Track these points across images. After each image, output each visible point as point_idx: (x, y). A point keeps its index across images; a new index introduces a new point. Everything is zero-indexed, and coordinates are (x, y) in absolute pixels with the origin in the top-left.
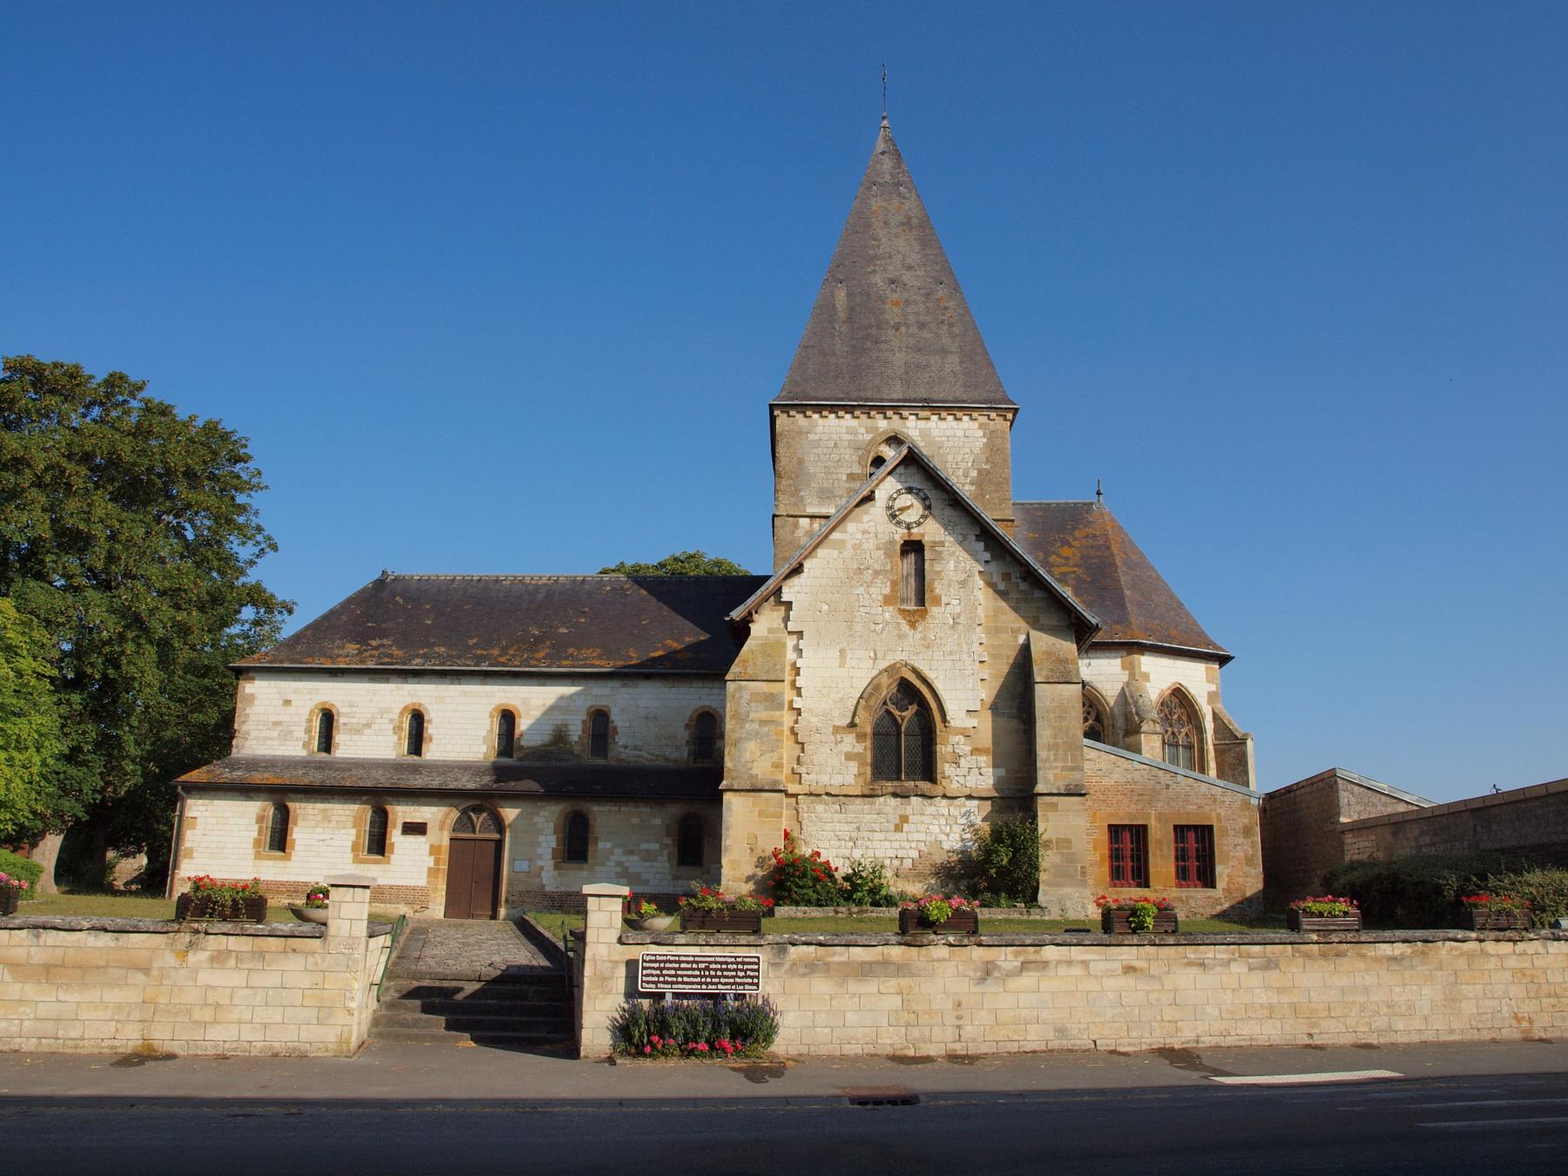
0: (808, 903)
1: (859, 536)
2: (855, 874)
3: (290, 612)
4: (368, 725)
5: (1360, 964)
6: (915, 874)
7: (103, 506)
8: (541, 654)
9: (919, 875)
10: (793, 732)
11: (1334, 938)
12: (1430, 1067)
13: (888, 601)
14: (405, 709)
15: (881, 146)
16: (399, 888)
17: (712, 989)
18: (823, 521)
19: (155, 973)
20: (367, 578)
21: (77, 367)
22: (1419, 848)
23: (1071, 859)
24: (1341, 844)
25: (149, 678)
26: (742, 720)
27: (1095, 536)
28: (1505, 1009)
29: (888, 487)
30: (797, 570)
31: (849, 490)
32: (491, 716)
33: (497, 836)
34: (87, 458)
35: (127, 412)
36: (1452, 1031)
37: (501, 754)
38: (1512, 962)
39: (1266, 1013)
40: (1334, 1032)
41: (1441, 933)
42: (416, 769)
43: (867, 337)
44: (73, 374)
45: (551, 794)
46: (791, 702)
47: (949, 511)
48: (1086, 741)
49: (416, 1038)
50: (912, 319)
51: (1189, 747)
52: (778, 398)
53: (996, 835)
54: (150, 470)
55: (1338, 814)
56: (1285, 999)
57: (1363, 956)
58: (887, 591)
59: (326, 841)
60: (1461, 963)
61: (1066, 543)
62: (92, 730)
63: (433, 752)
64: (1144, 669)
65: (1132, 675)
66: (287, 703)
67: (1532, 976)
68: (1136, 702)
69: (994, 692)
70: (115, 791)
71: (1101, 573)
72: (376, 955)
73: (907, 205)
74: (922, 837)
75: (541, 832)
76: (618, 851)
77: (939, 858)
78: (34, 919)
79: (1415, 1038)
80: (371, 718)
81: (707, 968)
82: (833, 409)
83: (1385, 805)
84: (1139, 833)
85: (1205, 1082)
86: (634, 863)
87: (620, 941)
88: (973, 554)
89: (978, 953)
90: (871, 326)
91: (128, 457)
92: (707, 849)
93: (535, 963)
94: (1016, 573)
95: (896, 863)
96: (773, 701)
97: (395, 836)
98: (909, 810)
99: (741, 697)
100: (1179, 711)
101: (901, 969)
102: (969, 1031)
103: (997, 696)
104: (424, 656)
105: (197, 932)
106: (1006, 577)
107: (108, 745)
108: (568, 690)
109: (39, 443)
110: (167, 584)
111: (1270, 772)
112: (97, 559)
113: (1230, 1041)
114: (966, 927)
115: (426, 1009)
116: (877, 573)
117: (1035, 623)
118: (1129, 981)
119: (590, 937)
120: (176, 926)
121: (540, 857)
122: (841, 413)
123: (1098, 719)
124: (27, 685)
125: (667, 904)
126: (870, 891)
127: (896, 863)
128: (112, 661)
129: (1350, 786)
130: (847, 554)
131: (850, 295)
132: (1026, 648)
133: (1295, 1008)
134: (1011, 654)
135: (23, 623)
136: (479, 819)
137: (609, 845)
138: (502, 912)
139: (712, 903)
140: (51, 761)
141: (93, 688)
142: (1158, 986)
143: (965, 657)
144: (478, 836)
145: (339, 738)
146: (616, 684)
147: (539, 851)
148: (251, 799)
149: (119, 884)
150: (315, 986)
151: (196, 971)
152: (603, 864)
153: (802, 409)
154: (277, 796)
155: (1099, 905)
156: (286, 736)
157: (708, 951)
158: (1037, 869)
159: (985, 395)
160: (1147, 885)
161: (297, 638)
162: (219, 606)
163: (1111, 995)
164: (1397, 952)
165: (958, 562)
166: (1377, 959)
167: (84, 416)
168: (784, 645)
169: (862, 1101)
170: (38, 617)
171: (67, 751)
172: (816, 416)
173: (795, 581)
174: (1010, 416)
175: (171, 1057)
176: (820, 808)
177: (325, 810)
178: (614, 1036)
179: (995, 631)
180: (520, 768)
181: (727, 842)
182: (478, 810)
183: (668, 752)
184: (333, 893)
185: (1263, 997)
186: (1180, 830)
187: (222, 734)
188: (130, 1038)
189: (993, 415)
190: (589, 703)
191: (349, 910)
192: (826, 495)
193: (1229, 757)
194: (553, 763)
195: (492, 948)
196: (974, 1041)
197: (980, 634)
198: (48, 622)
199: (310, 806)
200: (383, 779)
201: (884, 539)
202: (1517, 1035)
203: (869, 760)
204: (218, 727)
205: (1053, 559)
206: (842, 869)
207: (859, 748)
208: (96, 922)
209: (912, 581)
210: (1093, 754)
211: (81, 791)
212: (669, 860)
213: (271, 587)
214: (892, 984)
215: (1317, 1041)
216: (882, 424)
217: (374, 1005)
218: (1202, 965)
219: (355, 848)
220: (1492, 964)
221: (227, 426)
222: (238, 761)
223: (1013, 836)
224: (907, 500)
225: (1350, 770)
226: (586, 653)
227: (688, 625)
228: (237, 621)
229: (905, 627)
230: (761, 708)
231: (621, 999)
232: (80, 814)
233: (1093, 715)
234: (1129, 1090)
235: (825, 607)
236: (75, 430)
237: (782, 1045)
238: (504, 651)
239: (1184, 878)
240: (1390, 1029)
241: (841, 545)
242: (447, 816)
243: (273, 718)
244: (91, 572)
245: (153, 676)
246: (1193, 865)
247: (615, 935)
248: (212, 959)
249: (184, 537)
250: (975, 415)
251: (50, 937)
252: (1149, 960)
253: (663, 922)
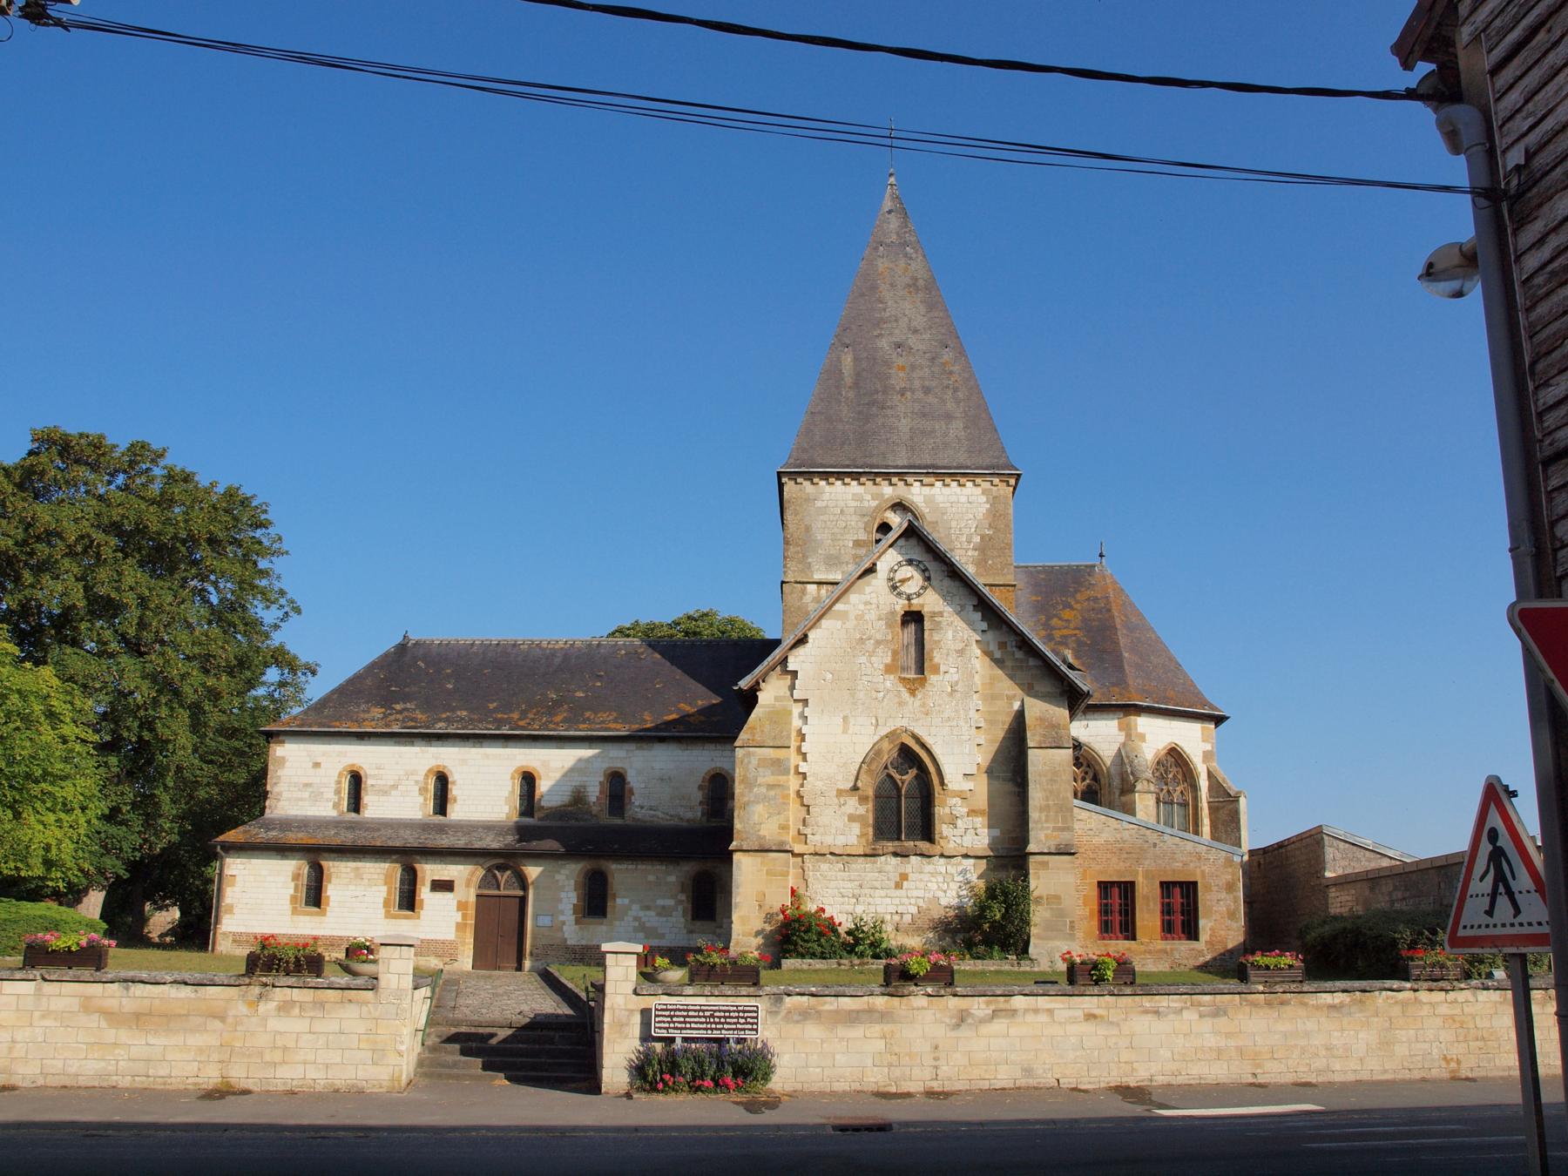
0: (813, 955)
1: (862, 607)
2: (857, 929)
3: (314, 673)
4: (395, 787)
5: (1302, 1012)
6: (913, 928)
7: (133, 575)
8: (559, 718)
9: (918, 929)
10: (799, 795)
11: (1278, 988)
12: (1353, 1102)
13: (889, 669)
14: (430, 771)
15: (888, 204)
16: (429, 942)
17: (716, 1034)
18: (830, 587)
19: (230, 1020)
20: (388, 643)
21: (101, 437)
22: (1392, 902)
23: (1061, 914)
24: (1326, 898)
25: (182, 741)
26: (750, 785)
27: (1096, 599)
28: (1435, 1051)
29: (890, 559)
30: (803, 640)
31: (855, 557)
32: (513, 778)
33: (521, 893)
34: (115, 528)
35: (151, 480)
36: (1385, 1071)
37: (522, 814)
38: (1444, 1010)
39: (1214, 1055)
40: (1276, 1072)
41: (1378, 984)
42: (441, 829)
43: (874, 403)
44: (97, 444)
45: (571, 853)
46: (797, 767)
47: (947, 582)
48: (1077, 802)
49: (457, 1077)
50: (917, 383)
51: (1184, 805)
52: (787, 465)
53: (991, 893)
54: (175, 537)
55: (1324, 869)
56: (1232, 1043)
57: (1306, 1004)
58: (888, 660)
59: (358, 901)
60: (1396, 1011)
61: (1068, 606)
62: (129, 792)
63: (458, 812)
64: (1140, 730)
65: (1128, 736)
66: (317, 765)
67: (1462, 1023)
68: (1131, 763)
69: (990, 757)
70: (150, 848)
71: (1101, 639)
72: (419, 1006)
73: (913, 265)
74: (921, 893)
76: (636, 907)
77: (937, 913)
78: (124, 974)
79: (1351, 1077)
80: (398, 779)
81: (712, 1016)
82: (840, 476)
83: (1369, 860)
84: (1127, 889)
85: (1147, 1114)
86: (651, 918)
87: (635, 993)
88: (970, 624)
89: (953, 1002)
90: (877, 392)
91: (154, 526)
92: (719, 905)
93: (560, 1012)
94: (1011, 641)
95: (896, 918)
96: (779, 766)
98: (908, 869)
99: (749, 761)
100: (1174, 770)
101: (885, 1016)
102: (945, 1070)
103: (993, 761)
104: (447, 720)
105: (266, 985)
106: (1002, 645)
107: (146, 806)
108: (586, 753)
109: (68, 514)
110: (196, 650)
111: (1257, 832)
112: (129, 622)
113: (1181, 1080)
114: (943, 978)
115: (464, 1052)
116: (878, 643)
117: (1030, 690)
118: (1089, 1028)
119: (609, 989)
120: (247, 980)
121: (562, 912)
122: (847, 480)
123: (1095, 778)
124: (72, 750)
125: (677, 956)
126: (872, 944)
127: (896, 918)
128: (147, 724)
129: (1335, 842)
130: (851, 624)
131: (856, 359)
132: (1020, 717)
133: (1240, 1050)
134: (1006, 720)
135: (66, 691)
136: (504, 877)
137: (626, 901)
138: (527, 964)
139: (716, 958)
140: (94, 821)
141: (131, 751)
142: (1115, 1031)
143: (962, 723)
144: (503, 892)
145: (367, 799)
146: (631, 746)
147: (560, 907)
149: (155, 936)
150: (369, 1032)
151: (265, 1019)
153: (809, 476)
154: (312, 856)
155: (1064, 960)
156: (316, 797)
157: (713, 1001)
158: (1028, 924)
159: (987, 461)
160: (1134, 938)
161: (324, 703)
162: (244, 668)
163: (1073, 1040)
164: (1337, 1001)
165: (955, 631)
166: (1318, 1007)
167: (109, 483)
168: (790, 713)
169: (843, 1129)
170: (75, 683)
171: (107, 811)
172: (823, 483)
173: (801, 650)
174: (1012, 482)
175: (246, 1092)
176: (824, 867)
178: (631, 1075)
179: (991, 698)
180: (544, 829)
181: (736, 899)
182: (502, 868)
183: (681, 812)
184: (384, 953)
185: (1212, 1041)
186: (1166, 886)
187: (253, 793)
188: (211, 1077)
189: (996, 480)
190: (605, 765)
191: (396, 966)
192: (832, 561)
193: (1223, 815)
194: (573, 823)
195: (517, 999)
196: (950, 1079)
197: (977, 702)
198: (85, 686)
200: (410, 839)
201: (885, 610)
202: (1446, 1075)
203: (871, 821)
204: (246, 786)
205: (1055, 621)
206: (845, 923)
207: (861, 810)
208: (177, 976)
209: (912, 650)
210: (1084, 815)
211: (121, 849)
213: (293, 648)
214: (877, 1029)
215: (1261, 1080)
216: (887, 491)
217: (418, 1048)
218: (1157, 1013)
219: (386, 904)
220: (1426, 1010)
221: (246, 491)
222: (272, 821)
223: (1005, 894)
224: (907, 571)
225: (1336, 825)
226: (603, 716)
227: (701, 689)
228: (264, 683)
229: (905, 695)
230: (768, 772)
231: (637, 1043)
232: (121, 872)
233: (1091, 774)
234: (1076, 1121)
235: (829, 676)
236: (100, 498)
237: (782, 1080)
238: (523, 715)
239: (1169, 931)
240: (1328, 1069)
241: (843, 616)
242: (473, 874)
243: (304, 779)
244: (123, 638)
245: (185, 739)
246: (1178, 919)
247: (630, 987)
248: (279, 1009)
249: (208, 601)
250: (978, 480)
251: (138, 989)
252: (1108, 1008)
253: (676, 975)
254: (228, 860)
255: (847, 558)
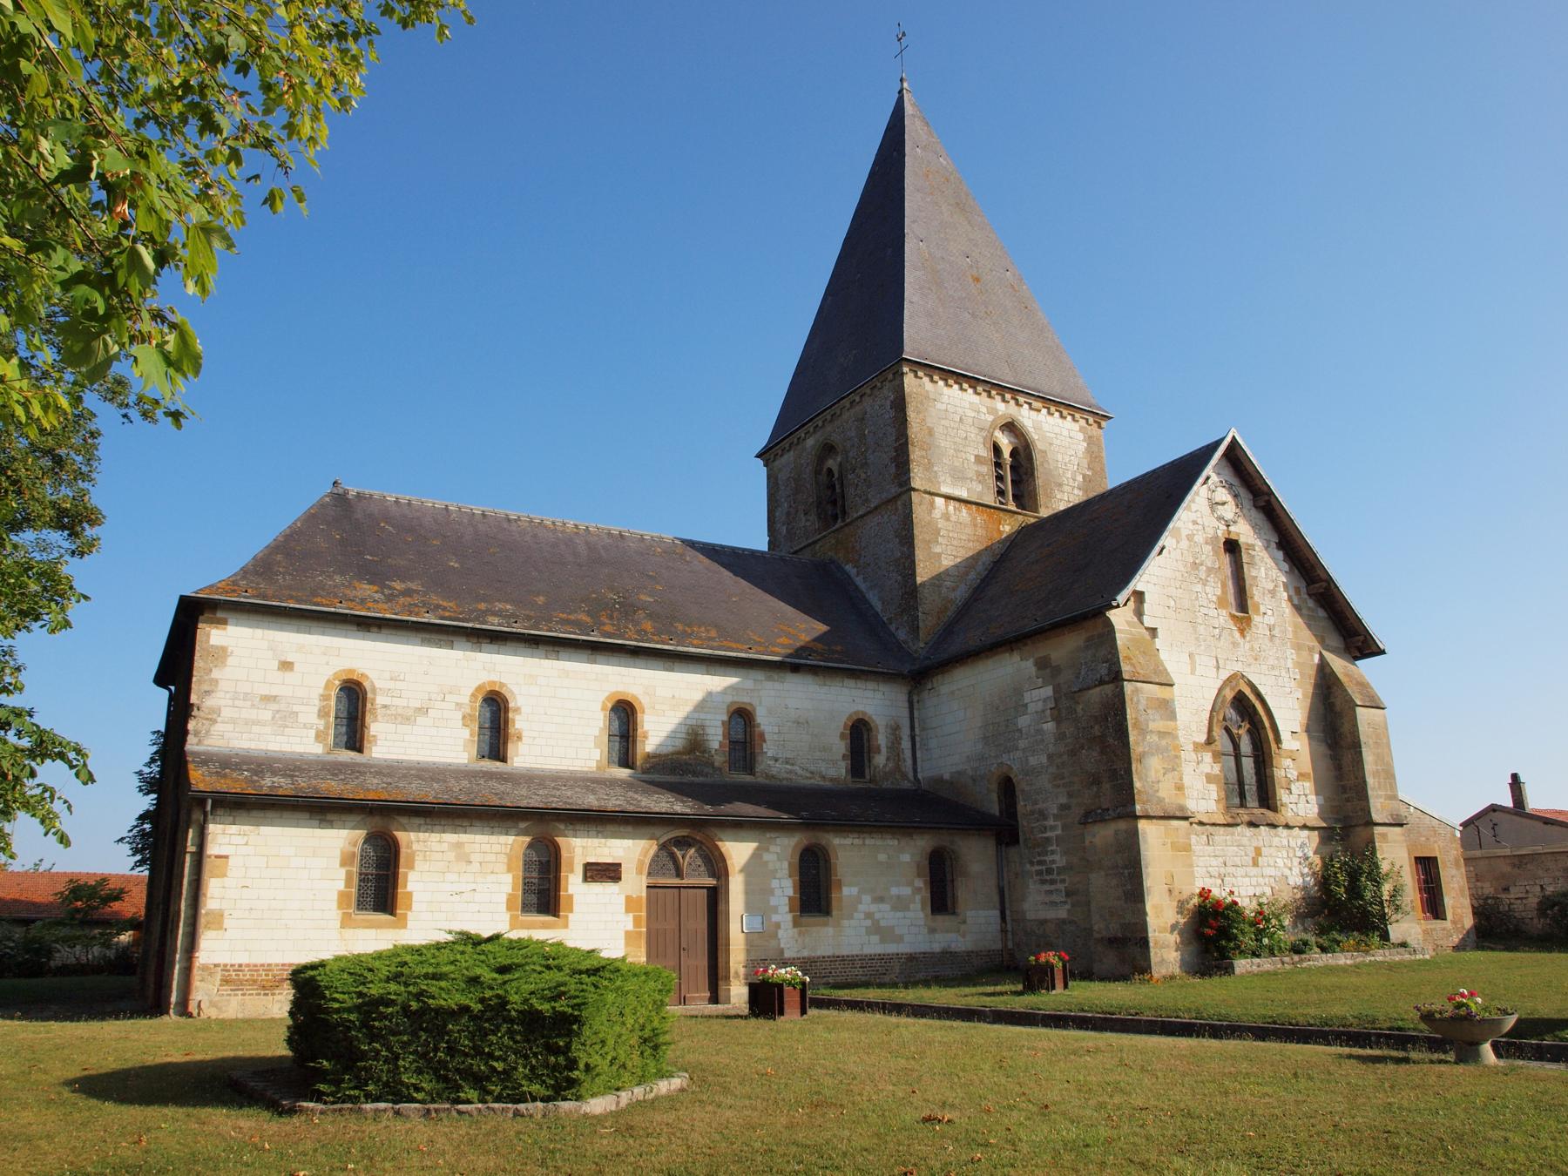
1: (1191, 526)
4: (423, 711)
63: (524, 755)
66: (286, 666)
75: (773, 874)
76: (867, 898)
97: (573, 883)
116: (1209, 570)
121: (775, 910)
137: (854, 890)
144: (685, 882)
145: (378, 728)
146: (759, 675)
147: (773, 901)
148: (330, 825)
152: (851, 918)
154: (377, 822)
156: (285, 719)
177: (459, 845)
182: (683, 843)
183: (823, 767)
190: (620, 689)
199: (435, 837)
201: (1211, 533)
212: (923, 909)
216: (1003, 408)
250: (1077, 416)
254: (213, 828)
255: (971, 474)
